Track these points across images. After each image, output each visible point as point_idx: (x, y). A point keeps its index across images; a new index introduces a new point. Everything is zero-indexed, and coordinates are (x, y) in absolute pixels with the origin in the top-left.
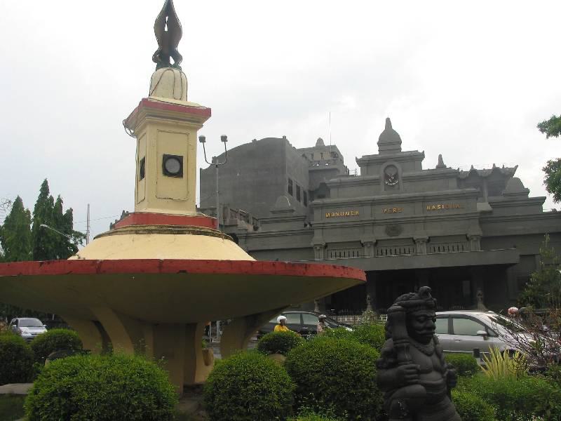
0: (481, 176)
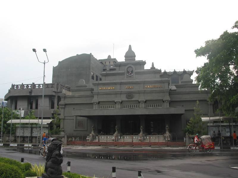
0: (169, 75)
